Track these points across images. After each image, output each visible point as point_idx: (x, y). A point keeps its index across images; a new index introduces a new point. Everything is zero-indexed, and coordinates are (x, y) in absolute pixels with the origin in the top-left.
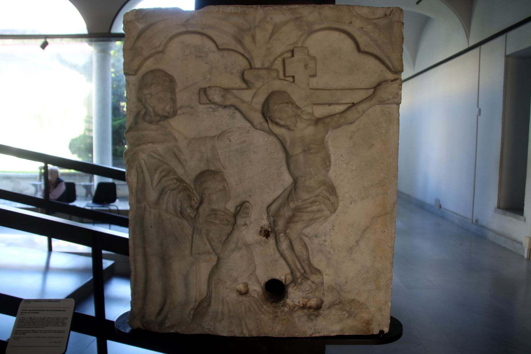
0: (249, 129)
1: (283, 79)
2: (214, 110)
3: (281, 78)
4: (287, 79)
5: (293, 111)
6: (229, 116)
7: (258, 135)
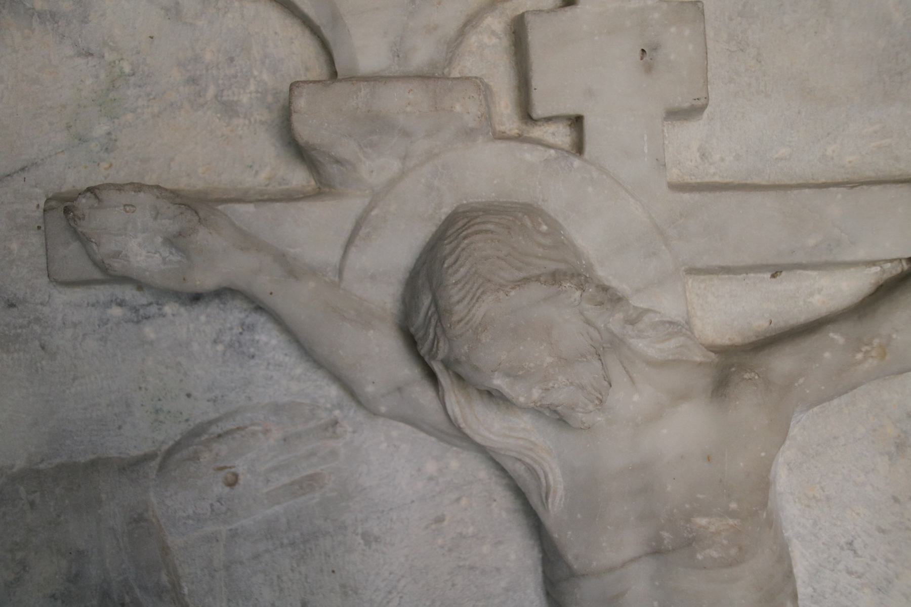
0: (337, 413)
1: (515, 132)
2: (139, 317)
3: (502, 128)
4: (537, 132)
5: (588, 322)
6: (220, 348)
7: (384, 446)
